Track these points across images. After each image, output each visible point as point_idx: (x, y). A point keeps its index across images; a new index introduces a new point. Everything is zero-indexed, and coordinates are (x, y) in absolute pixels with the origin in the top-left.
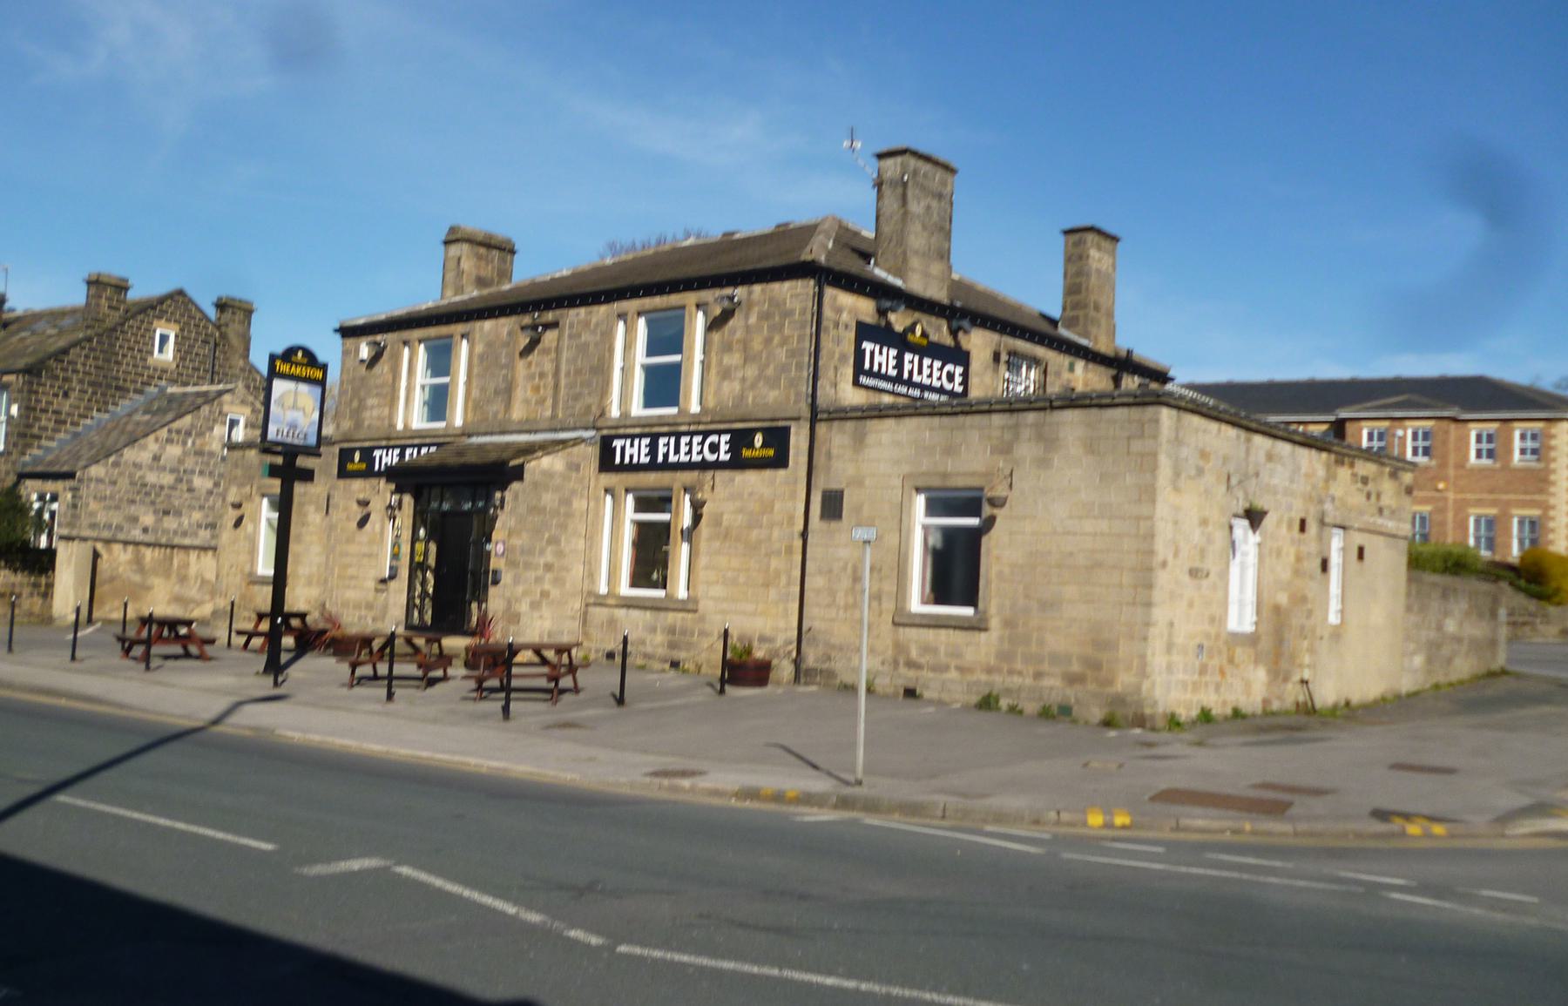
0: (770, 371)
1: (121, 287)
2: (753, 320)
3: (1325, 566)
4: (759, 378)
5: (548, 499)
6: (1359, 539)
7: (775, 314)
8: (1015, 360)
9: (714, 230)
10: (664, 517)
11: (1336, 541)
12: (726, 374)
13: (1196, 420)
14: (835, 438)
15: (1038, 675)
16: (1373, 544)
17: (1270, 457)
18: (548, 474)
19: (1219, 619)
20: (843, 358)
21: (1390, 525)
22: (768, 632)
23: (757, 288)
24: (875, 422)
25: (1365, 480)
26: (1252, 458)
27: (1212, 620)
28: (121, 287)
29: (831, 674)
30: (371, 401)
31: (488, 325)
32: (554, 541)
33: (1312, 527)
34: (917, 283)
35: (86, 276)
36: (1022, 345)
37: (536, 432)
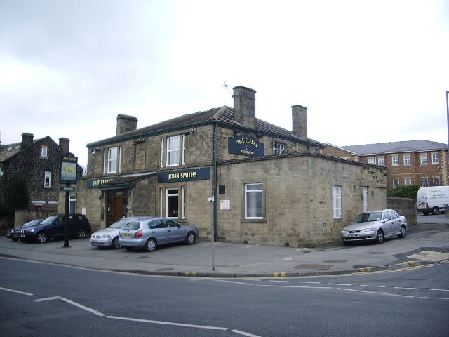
0: (203, 152)
1: (32, 136)
2: (198, 138)
3: (362, 198)
4: (201, 154)
5: (143, 192)
6: (371, 189)
7: (203, 137)
8: (276, 145)
9: (192, 111)
10: (177, 195)
11: (365, 191)
12: (191, 154)
13: (320, 160)
14: (222, 171)
15: (280, 235)
16: (377, 191)
17: (343, 169)
18: (144, 185)
19: (329, 215)
20: (224, 147)
21: (382, 185)
22: (206, 227)
23: (198, 128)
24: (232, 165)
25: (372, 173)
26: (338, 169)
27: (328, 216)
28: (32, 136)
29: (224, 238)
30: (96, 166)
31: (127, 143)
32: (146, 204)
33: (357, 187)
34: (246, 125)
35: (61, 137)
36: (279, 140)
37: (141, 173)
